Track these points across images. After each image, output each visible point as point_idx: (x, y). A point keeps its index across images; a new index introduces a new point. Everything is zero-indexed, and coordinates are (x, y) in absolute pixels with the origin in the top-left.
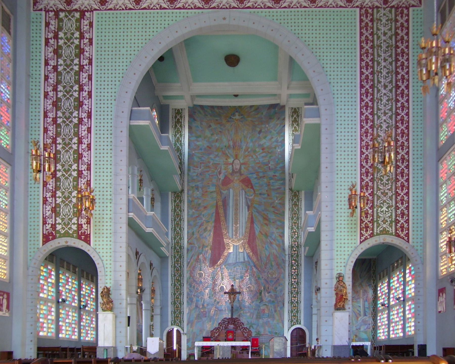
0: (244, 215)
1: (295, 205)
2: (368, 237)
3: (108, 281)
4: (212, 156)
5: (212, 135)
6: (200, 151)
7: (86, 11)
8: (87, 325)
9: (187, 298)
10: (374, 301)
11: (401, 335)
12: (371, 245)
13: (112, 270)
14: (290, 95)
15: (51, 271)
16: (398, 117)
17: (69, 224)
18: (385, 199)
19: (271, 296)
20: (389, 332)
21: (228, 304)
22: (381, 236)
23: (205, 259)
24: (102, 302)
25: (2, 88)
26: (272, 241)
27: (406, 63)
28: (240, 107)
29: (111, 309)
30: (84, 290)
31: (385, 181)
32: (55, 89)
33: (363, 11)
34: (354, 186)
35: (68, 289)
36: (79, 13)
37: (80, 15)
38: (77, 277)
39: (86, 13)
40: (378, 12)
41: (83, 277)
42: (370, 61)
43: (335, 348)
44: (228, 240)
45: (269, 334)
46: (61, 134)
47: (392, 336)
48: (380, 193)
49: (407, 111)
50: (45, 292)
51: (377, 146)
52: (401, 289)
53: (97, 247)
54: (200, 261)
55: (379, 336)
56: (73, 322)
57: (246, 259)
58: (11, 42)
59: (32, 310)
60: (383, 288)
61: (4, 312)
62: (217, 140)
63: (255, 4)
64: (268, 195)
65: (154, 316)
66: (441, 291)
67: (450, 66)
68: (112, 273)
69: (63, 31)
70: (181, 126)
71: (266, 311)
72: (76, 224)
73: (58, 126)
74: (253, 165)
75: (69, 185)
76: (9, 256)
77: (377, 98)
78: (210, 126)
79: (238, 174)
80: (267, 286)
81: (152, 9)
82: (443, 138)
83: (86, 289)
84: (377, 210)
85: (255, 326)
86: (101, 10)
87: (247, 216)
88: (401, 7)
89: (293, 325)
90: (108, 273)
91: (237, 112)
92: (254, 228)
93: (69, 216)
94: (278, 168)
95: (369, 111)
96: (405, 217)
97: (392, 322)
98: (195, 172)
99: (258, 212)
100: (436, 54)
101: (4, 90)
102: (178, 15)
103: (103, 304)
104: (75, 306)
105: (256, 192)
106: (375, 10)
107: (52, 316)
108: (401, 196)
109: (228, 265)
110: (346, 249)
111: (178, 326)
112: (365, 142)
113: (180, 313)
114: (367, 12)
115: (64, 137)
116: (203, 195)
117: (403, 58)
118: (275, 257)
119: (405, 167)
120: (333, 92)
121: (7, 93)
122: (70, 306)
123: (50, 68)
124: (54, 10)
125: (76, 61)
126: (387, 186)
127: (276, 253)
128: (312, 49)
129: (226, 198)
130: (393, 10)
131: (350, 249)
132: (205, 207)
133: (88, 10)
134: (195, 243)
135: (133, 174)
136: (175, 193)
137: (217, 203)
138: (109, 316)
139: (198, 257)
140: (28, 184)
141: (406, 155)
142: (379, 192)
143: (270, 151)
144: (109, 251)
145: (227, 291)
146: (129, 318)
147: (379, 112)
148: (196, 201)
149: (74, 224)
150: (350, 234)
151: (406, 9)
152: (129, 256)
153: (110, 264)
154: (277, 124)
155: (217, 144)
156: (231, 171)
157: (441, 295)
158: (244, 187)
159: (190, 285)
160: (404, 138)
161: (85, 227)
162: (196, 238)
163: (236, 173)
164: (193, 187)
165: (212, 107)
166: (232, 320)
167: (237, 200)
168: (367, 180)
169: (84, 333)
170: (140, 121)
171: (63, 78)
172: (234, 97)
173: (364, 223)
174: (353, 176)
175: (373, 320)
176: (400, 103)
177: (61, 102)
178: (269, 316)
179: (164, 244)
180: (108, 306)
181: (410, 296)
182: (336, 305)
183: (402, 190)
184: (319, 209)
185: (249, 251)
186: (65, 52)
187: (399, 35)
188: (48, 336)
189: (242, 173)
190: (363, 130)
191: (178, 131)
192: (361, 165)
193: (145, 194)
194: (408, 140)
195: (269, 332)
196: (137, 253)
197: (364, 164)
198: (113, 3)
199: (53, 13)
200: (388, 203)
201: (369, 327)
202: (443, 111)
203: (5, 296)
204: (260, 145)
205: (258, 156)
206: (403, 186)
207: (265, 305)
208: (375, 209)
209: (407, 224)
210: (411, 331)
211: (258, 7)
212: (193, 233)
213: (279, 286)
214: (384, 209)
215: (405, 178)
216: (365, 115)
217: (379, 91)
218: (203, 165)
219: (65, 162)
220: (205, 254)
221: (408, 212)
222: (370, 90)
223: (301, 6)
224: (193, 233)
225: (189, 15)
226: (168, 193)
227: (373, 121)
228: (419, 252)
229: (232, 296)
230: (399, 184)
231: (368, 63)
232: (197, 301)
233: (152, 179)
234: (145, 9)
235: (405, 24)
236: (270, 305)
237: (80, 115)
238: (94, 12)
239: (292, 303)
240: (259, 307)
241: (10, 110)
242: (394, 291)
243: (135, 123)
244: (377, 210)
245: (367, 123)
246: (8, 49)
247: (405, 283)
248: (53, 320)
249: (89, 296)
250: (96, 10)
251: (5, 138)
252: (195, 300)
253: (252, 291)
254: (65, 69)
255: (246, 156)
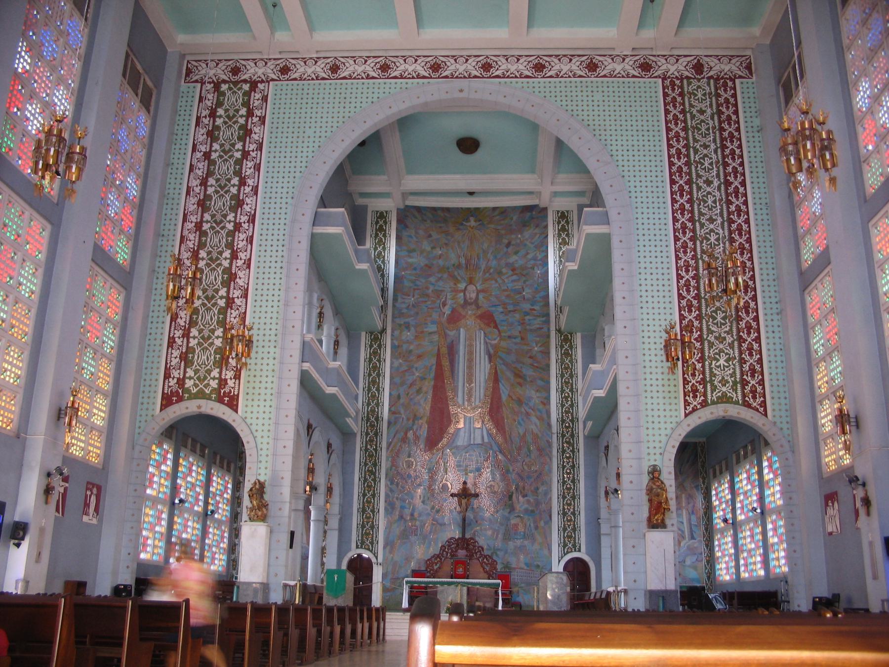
0: (483, 369)
1: (567, 354)
2: (699, 407)
3: (262, 471)
4: (432, 279)
5: (433, 248)
6: (414, 272)
7: (259, 82)
8: (214, 543)
9: (386, 501)
10: (705, 513)
11: (762, 573)
12: (703, 420)
13: (269, 453)
14: (555, 193)
15: (167, 452)
16: (733, 225)
17: (205, 378)
18: (721, 346)
19: (528, 501)
20: (737, 567)
21: (455, 514)
22: (719, 405)
23: (417, 438)
24: (250, 505)
25: (129, 182)
26: (530, 411)
27: (738, 151)
28: (477, 209)
29: (263, 518)
30: (214, 484)
31: (719, 319)
32: (204, 183)
33: (668, 82)
34: (672, 327)
35: (190, 482)
36: (248, 85)
37: (251, 87)
38: (205, 464)
39: (259, 85)
40: (689, 84)
41: (215, 463)
42: (683, 147)
43: (652, 595)
44: (455, 408)
45: (526, 568)
46: (206, 246)
47: (745, 575)
48: (713, 338)
49: (746, 217)
50: (155, 486)
51: (714, 266)
52: (756, 495)
53: (249, 415)
54: (409, 443)
55: (719, 575)
56: (194, 538)
57: (486, 440)
58: (149, 123)
59: (133, 515)
60: (721, 491)
61: (91, 517)
62: (440, 257)
63: (507, 72)
64: (522, 339)
65: (329, 533)
66: (830, 498)
67: (832, 155)
68: (270, 458)
69: (224, 107)
70: (385, 236)
71: (521, 529)
72: (217, 378)
73: (203, 234)
74: (498, 293)
75: (212, 319)
76: (106, 426)
77: (697, 199)
78: (430, 236)
79: (473, 307)
80: (521, 484)
81: (355, 78)
82: (808, 256)
83: (218, 483)
84: (710, 364)
85: (500, 554)
86: (280, 80)
87: (487, 371)
88: (722, 78)
89: (568, 552)
90: (263, 459)
91: (472, 216)
92: (499, 389)
93: (207, 366)
94: (538, 299)
95: (687, 216)
96: (756, 375)
97: (743, 551)
98: (404, 303)
99: (506, 364)
100: (810, 138)
101: (130, 184)
102: (393, 86)
103: (252, 509)
104: (197, 512)
105: (503, 334)
106: (685, 81)
107: (162, 526)
108: (747, 343)
109: (456, 449)
110: (662, 426)
111: (368, 549)
112: (683, 260)
113: (372, 527)
114: (673, 84)
115: (210, 249)
116: (416, 336)
117: (732, 145)
118: (536, 437)
119: (750, 299)
120: (630, 189)
121: (134, 189)
122: (191, 510)
123: (199, 155)
124: (213, 81)
125: (239, 146)
126: (723, 327)
127: (536, 431)
128: (594, 130)
129: (454, 343)
130: (712, 81)
131: (669, 426)
132: (419, 357)
133: (262, 80)
134: (402, 411)
135: (310, 304)
136: (371, 333)
137: (439, 350)
138: (261, 529)
139: (406, 434)
140: (148, 316)
141: (751, 280)
142: (710, 335)
143: (524, 272)
144: (267, 422)
145: (455, 491)
146: (292, 534)
147: (702, 218)
148: (405, 346)
149: (214, 379)
150: (667, 401)
151: (730, 81)
152: (297, 432)
153: (268, 443)
154: (536, 234)
155: (441, 262)
156: (462, 302)
157: (831, 504)
158: (482, 325)
159: (391, 480)
160: (745, 256)
161: (231, 383)
162: (403, 404)
163: (471, 304)
164: (400, 325)
165: (434, 209)
166: (465, 543)
167: (471, 345)
168: (690, 317)
169: (208, 557)
170: (328, 228)
171: (217, 168)
172: (468, 195)
173: (690, 384)
174: (668, 311)
175: (707, 546)
176: (734, 205)
177: (211, 200)
178: (525, 537)
179: (353, 413)
180: (260, 513)
181: (773, 505)
182: (649, 520)
183: (749, 333)
184: (613, 361)
185: (490, 425)
186: (224, 134)
187: (723, 113)
188: (153, 561)
189: (480, 305)
190: (679, 244)
191: (381, 243)
192: (680, 295)
193: (325, 334)
194: (751, 259)
195: (526, 564)
196: (309, 426)
197: (685, 294)
198: (298, 71)
199: (212, 85)
200: (727, 354)
201: (700, 559)
202: (804, 217)
203: (95, 491)
204: (507, 264)
205: (506, 280)
206: (749, 327)
207: (519, 516)
208: (707, 363)
209: (761, 387)
210: (780, 564)
211: (512, 75)
212: (399, 397)
213: (543, 484)
214: (722, 362)
215: (752, 315)
216: (680, 222)
217: (699, 188)
218: (417, 292)
219: (208, 286)
220: (417, 430)
221: (762, 367)
222: (686, 187)
223: (574, 76)
224: (399, 397)
225: (409, 86)
226: (360, 334)
227: (694, 231)
228: (786, 432)
229: (464, 501)
230: (743, 324)
231: (680, 150)
232: (402, 508)
233: (337, 312)
234: (344, 78)
235: (732, 100)
236: (526, 517)
237: (238, 219)
238: (271, 83)
239: (564, 514)
240: (509, 519)
241: (135, 213)
242: (742, 497)
243: (319, 230)
244: (710, 364)
245: (684, 233)
246: (144, 131)
247: (762, 485)
248: (162, 534)
249: (221, 496)
250: (273, 80)
251: (123, 250)
252: (398, 504)
253: (495, 493)
254: (221, 157)
255: (487, 280)
